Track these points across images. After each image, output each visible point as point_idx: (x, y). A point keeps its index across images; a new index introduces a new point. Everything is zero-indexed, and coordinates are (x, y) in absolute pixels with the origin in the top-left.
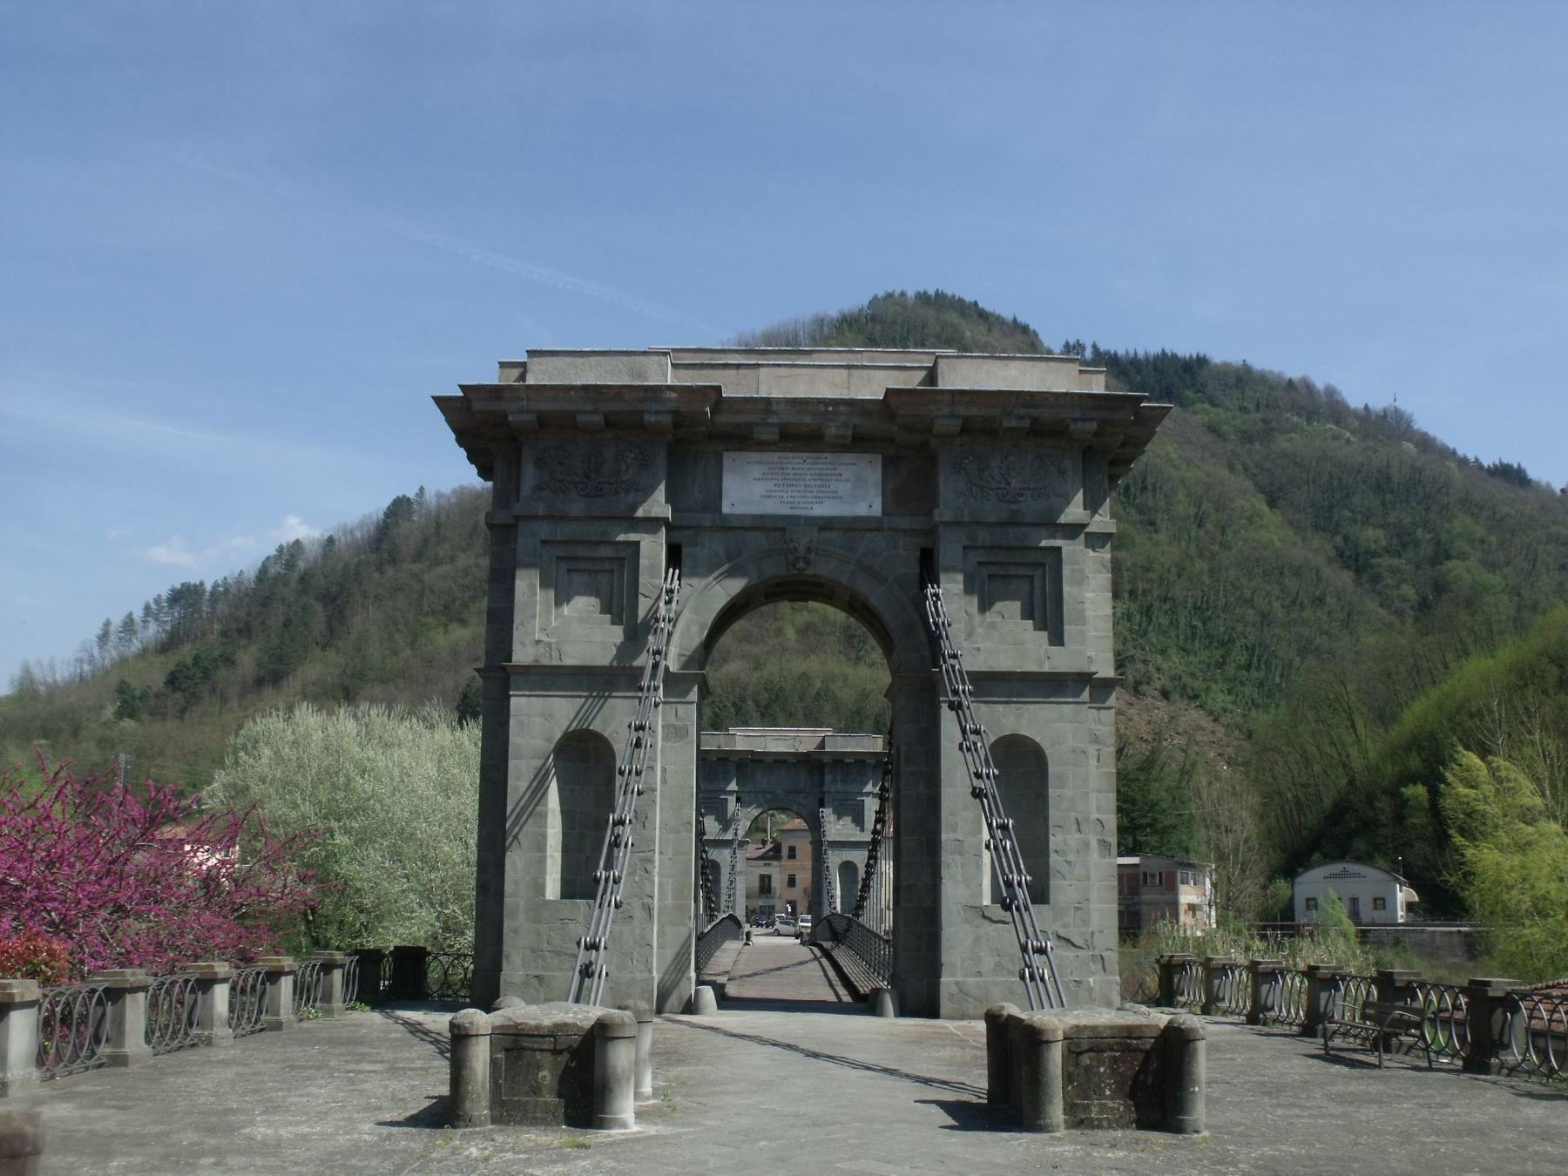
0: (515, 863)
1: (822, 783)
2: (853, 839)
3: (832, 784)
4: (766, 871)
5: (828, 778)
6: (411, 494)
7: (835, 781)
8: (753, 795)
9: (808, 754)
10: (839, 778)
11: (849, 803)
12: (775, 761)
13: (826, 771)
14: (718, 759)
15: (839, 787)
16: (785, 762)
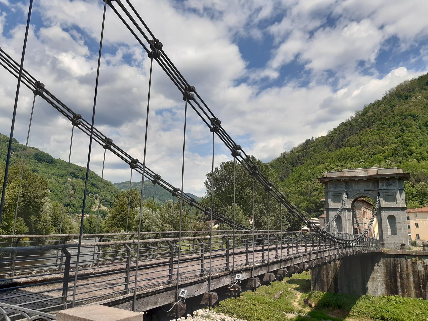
0: (384, 233)
1: (378, 187)
2: (392, 207)
3: (382, 186)
5: (380, 185)
6: (310, 138)
7: (383, 186)
8: (352, 192)
9: (371, 176)
10: (385, 184)
11: (390, 193)
12: (359, 180)
13: (379, 181)
14: (337, 180)
15: (385, 187)
16: (363, 180)
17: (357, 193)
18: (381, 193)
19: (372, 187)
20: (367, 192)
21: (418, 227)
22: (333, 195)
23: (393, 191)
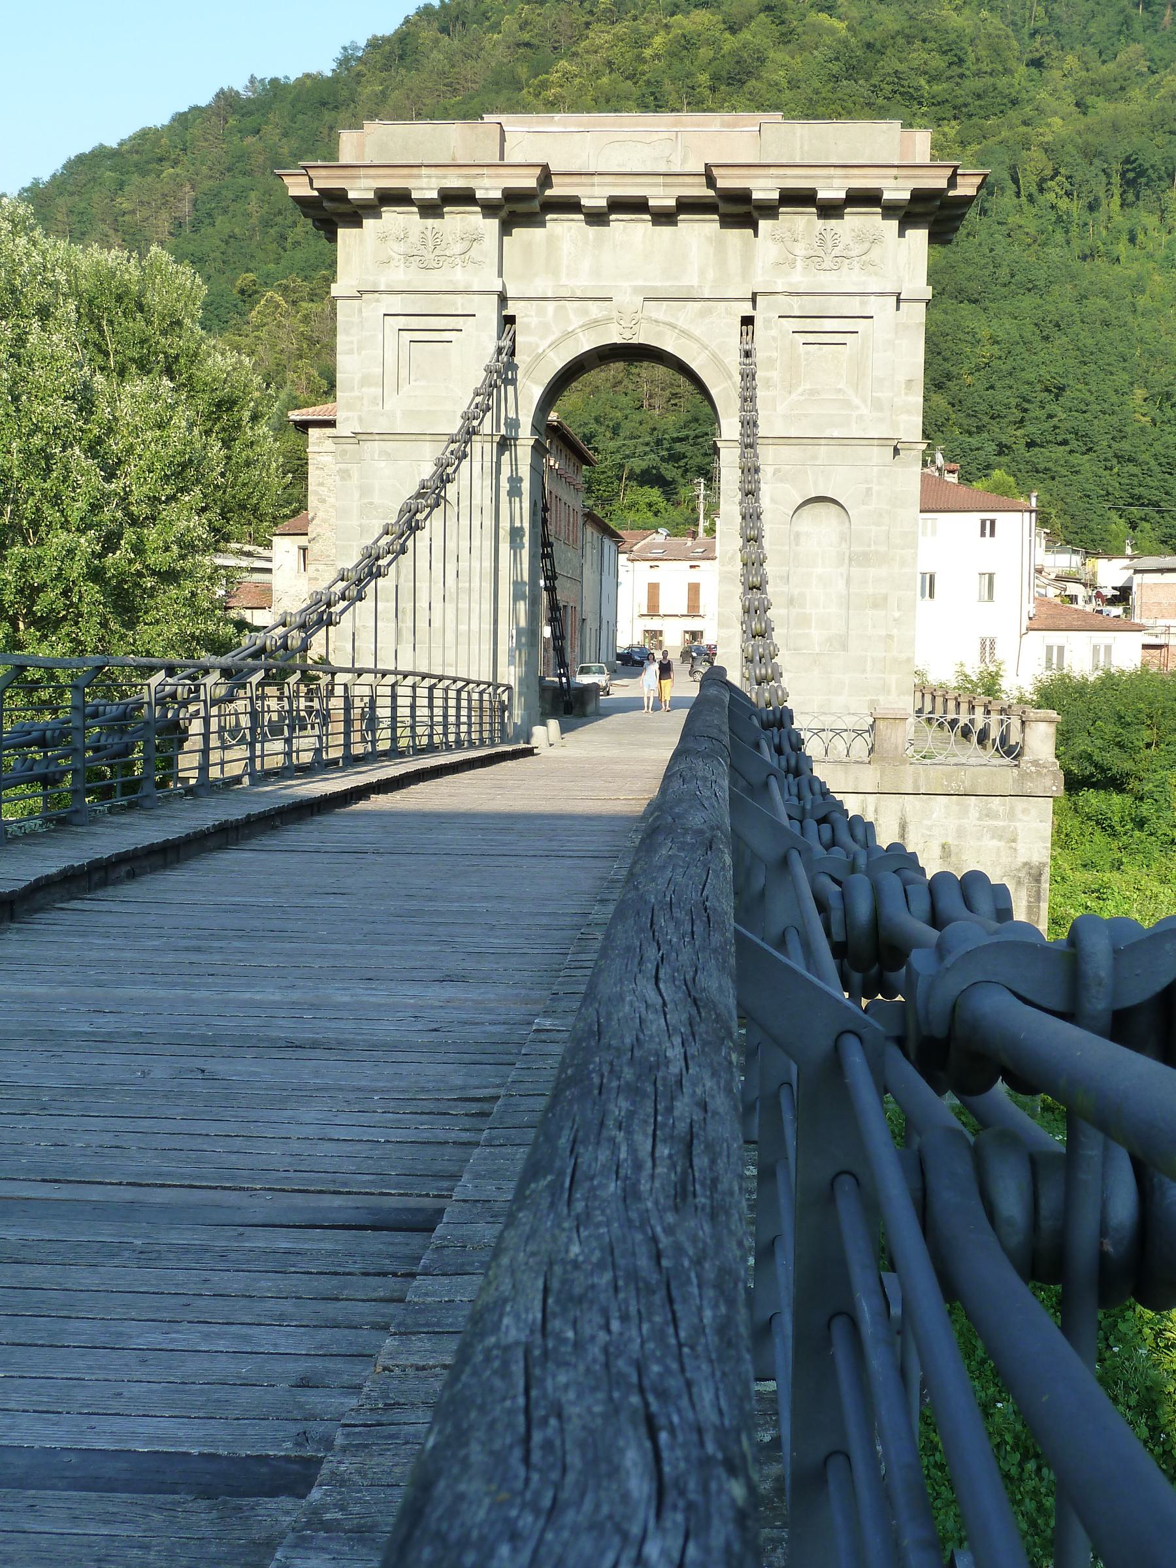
4: (694, 576)
7: (786, 263)
17: (586, 312)
18: (767, 321)
19: (702, 273)
20: (659, 311)
21: (992, 534)
22: (403, 322)
23: (853, 306)
